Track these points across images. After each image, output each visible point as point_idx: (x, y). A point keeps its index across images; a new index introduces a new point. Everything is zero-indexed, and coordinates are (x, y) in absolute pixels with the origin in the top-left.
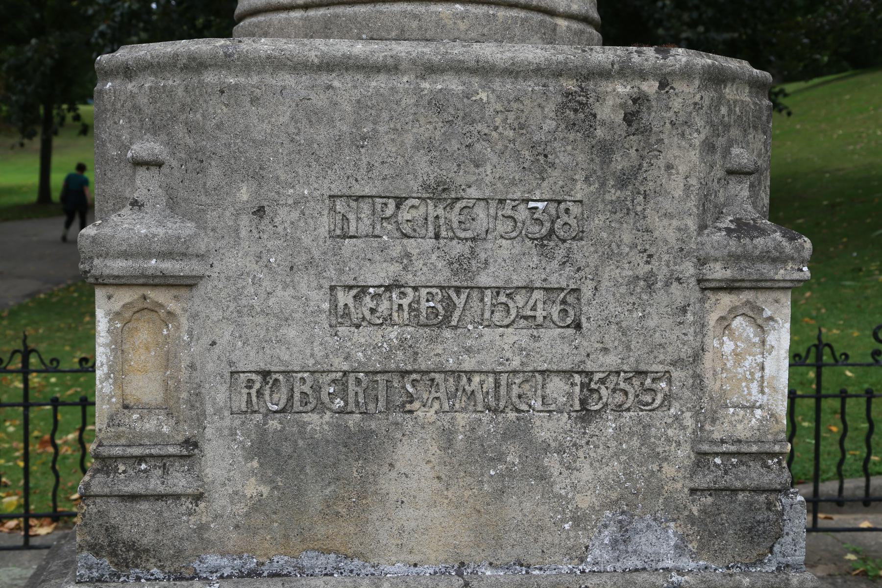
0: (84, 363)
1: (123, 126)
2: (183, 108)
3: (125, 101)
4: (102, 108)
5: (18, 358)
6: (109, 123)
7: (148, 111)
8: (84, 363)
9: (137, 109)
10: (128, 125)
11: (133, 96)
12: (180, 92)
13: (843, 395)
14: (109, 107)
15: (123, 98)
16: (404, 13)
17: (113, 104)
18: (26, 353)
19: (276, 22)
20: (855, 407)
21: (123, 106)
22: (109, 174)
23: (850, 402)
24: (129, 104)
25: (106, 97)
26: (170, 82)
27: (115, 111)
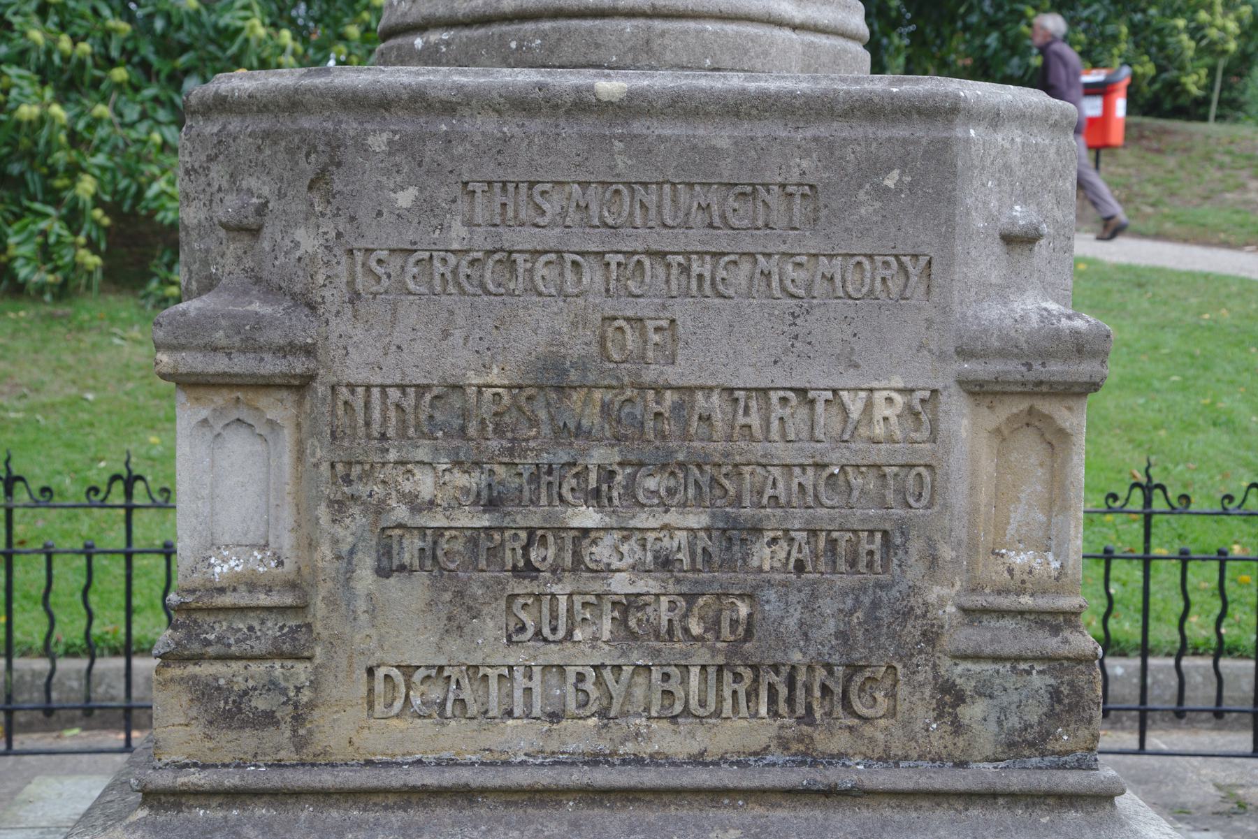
0: (92, 493)
1: (991, 189)
2: (1052, 177)
3: (995, 158)
4: (969, 163)
5: (119, 487)
6: (976, 184)
7: (1019, 172)
8: (92, 493)
9: (1007, 168)
10: (997, 189)
11: (1004, 152)
12: (1052, 153)
13: (1184, 558)
14: (976, 163)
15: (993, 153)
16: (738, 34)
17: (982, 160)
18: (130, 481)
19: (780, 41)
20: (1203, 576)
21: (992, 163)
22: (974, 253)
23: (1118, 568)
24: (999, 162)
25: (974, 149)
26: (1039, 140)
27: (983, 169)
